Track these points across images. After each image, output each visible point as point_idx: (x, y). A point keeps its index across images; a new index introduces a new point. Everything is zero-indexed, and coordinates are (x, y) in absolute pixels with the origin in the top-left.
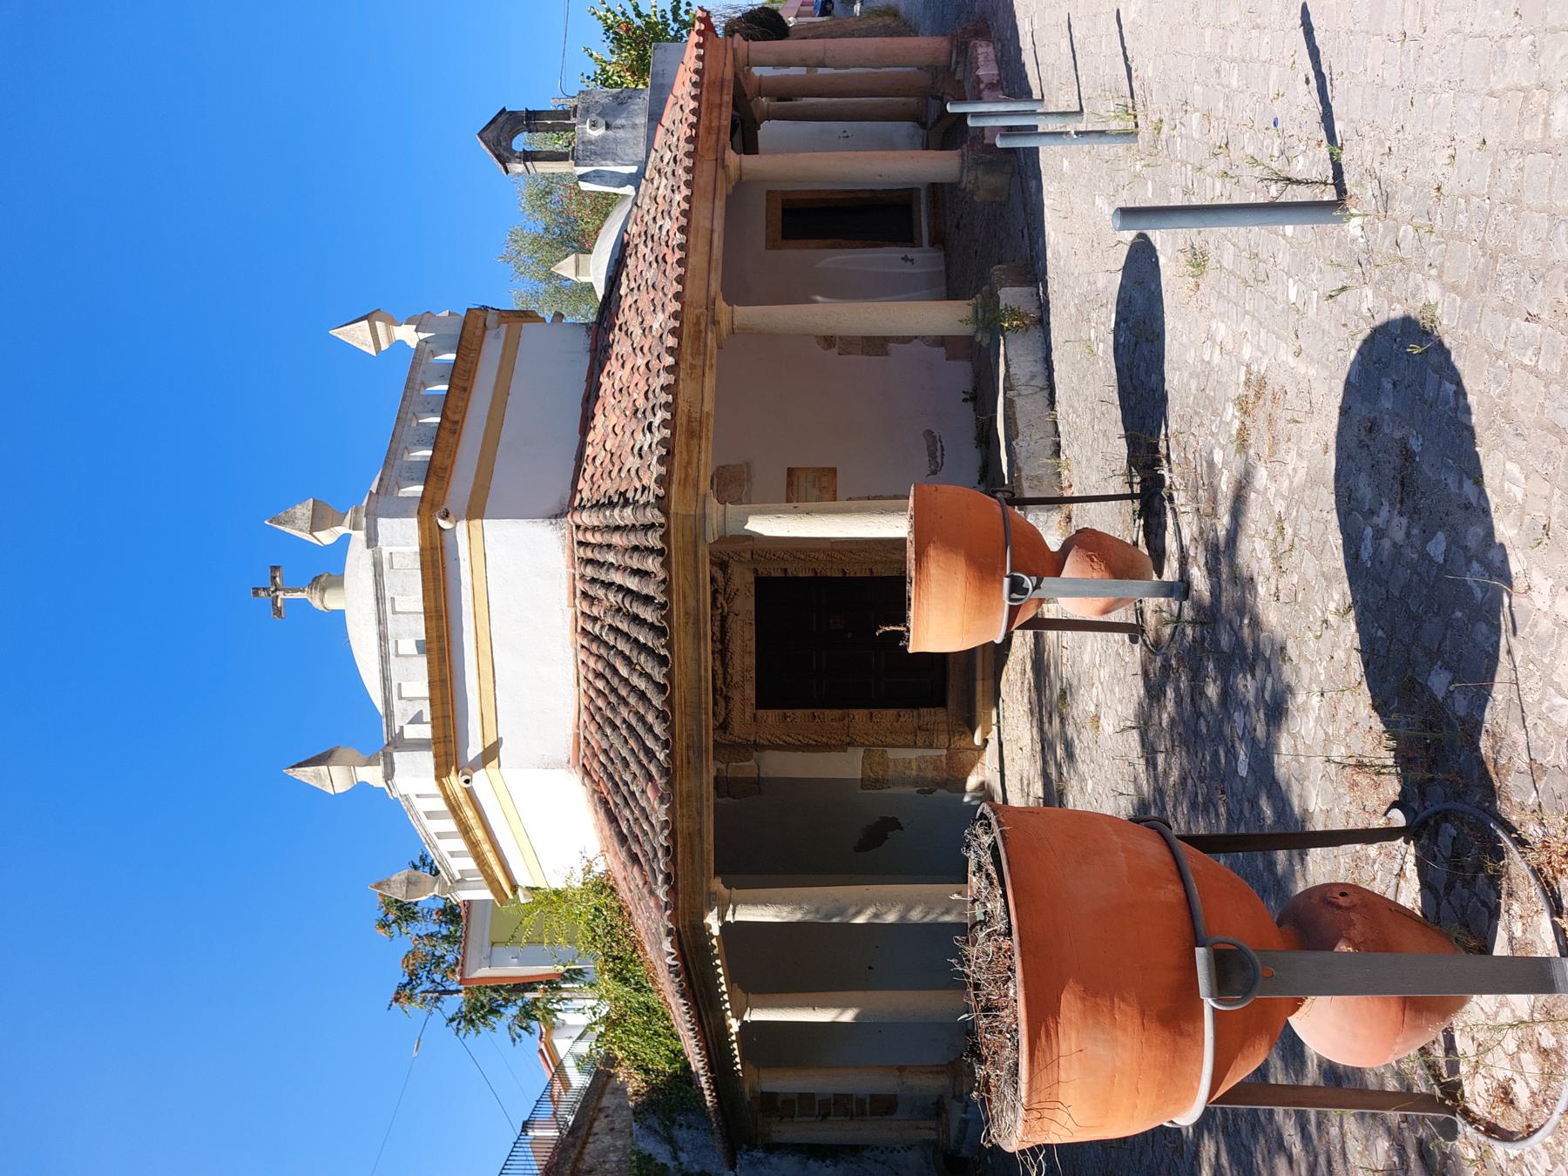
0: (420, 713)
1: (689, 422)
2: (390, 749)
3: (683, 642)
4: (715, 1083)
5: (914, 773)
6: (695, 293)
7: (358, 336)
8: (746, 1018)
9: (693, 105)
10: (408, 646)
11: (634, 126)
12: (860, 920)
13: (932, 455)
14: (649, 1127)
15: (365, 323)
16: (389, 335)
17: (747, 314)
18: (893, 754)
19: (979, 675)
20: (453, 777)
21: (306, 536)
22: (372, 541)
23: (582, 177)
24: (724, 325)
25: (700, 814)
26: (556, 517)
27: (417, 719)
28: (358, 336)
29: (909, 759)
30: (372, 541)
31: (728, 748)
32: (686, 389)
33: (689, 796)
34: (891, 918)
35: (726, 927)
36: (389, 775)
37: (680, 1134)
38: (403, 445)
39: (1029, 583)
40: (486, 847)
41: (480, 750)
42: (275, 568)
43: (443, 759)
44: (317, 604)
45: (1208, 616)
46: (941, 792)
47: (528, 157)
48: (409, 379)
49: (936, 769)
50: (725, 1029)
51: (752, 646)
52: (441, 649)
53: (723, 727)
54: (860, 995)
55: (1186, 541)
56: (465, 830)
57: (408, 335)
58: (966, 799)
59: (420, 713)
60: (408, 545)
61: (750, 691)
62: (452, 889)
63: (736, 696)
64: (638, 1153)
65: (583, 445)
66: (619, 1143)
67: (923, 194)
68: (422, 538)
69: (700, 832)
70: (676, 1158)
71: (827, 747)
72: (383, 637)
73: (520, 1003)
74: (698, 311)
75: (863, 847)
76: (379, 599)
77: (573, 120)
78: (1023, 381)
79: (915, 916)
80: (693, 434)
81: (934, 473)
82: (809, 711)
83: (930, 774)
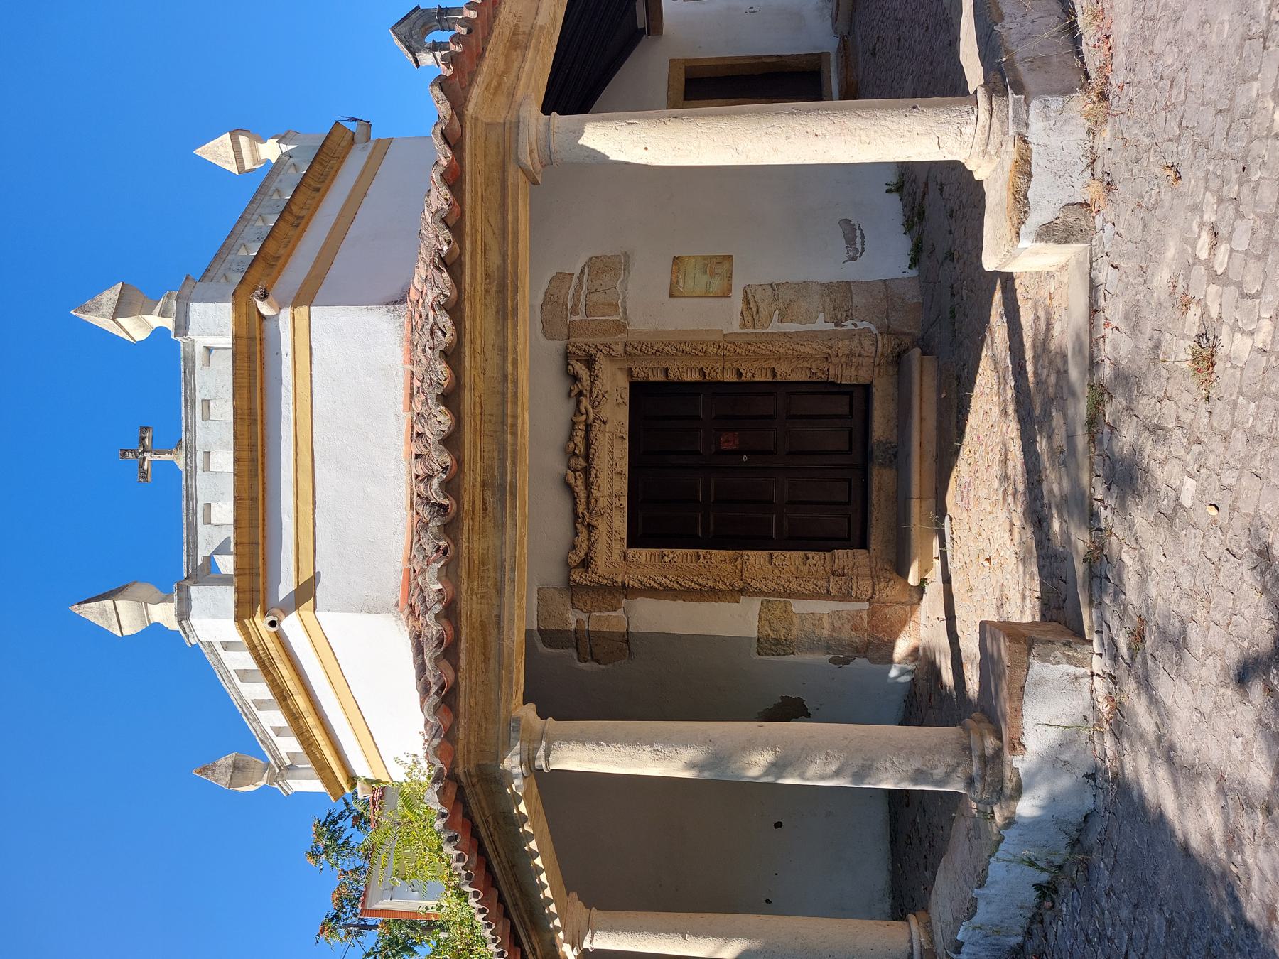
2: (187, 583)
5: (826, 633)
8: (586, 945)
16: (254, 153)
18: (798, 606)
19: (915, 490)
21: (106, 324)
26: (395, 303)
28: (219, 151)
29: (817, 614)
33: (483, 563)
36: (183, 614)
38: (240, 241)
40: (311, 721)
41: (293, 587)
42: (144, 429)
43: (248, 596)
46: (860, 663)
48: (262, 186)
49: (854, 628)
51: (624, 466)
54: (751, 920)
56: (282, 696)
58: (894, 673)
60: (221, 334)
61: (620, 523)
63: (602, 526)
67: (833, 58)
83: (847, 635)
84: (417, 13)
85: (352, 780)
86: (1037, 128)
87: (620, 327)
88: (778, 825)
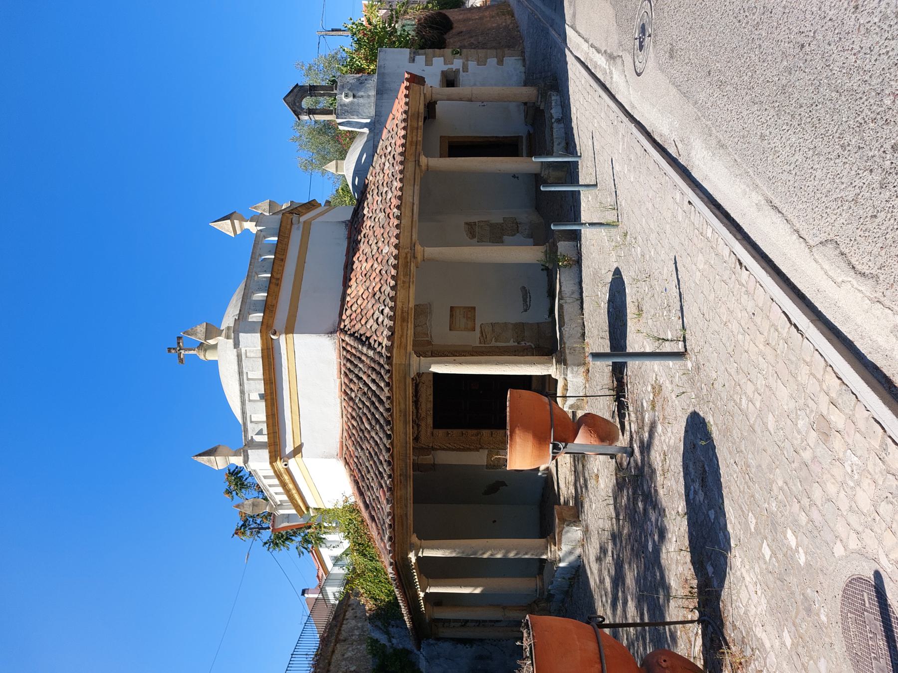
0: (262, 430)
1: (402, 313)
2: (246, 448)
3: (398, 425)
4: (412, 619)
6: (405, 241)
7: (225, 227)
9: (403, 133)
10: (255, 396)
11: (369, 96)
12: (485, 556)
13: (525, 300)
14: (376, 626)
15: (229, 221)
16: (241, 226)
17: (432, 252)
20: (278, 462)
22: (236, 345)
23: (340, 124)
24: (419, 257)
25: (406, 507)
26: (331, 333)
27: (260, 433)
30: (236, 345)
31: (420, 450)
32: (401, 294)
34: (499, 556)
35: (419, 559)
36: (246, 461)
37: (393, 630)
39: (561, 446)
40: (294, 492)
44: (202, 357)
45: (640, 470)
47: (311, 112)
48: (253, 253)
50: (417, 596)
52: (272, 399)
53: (416, 439)
55: (633, 430)
57: (251, 226)
59: (262, 430)
61: (430, 421)
62: (276, 509)
63: (423, 424)
64: (371, 638)
65: (344, 295)
66: (359, 625)
68: (263, 344)
69: (406, 514)
70: (390, 641)
71: (469, 450)
72: (242, 392)
73: (302, 534)
74: (406, 250)
75: (486, 493)
76: (240, 373)
77: (335, 92)
78: (568, 295)
79: (511, 555)
80: (404, 320)
81: (526, 311)
82: (460, 431)
84: (297, 89)
85: (308, 508)
86: (570, 376)
87: (429, 343)
88: (495, 521)
